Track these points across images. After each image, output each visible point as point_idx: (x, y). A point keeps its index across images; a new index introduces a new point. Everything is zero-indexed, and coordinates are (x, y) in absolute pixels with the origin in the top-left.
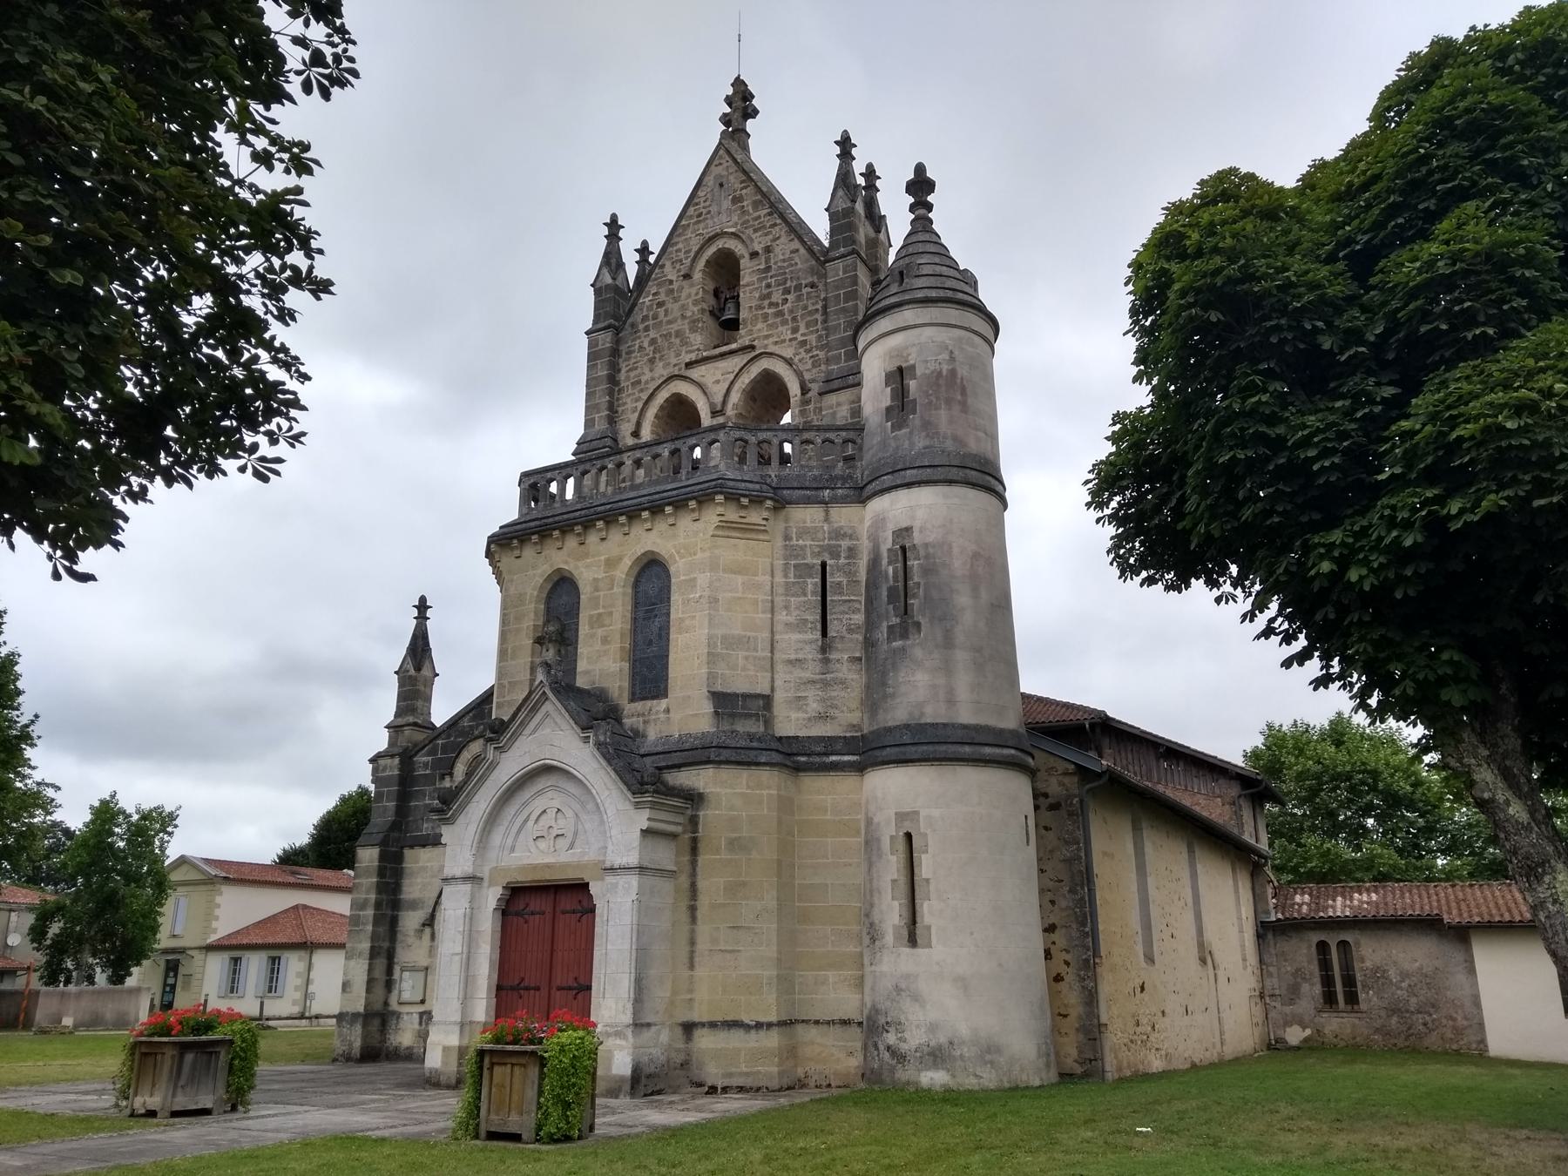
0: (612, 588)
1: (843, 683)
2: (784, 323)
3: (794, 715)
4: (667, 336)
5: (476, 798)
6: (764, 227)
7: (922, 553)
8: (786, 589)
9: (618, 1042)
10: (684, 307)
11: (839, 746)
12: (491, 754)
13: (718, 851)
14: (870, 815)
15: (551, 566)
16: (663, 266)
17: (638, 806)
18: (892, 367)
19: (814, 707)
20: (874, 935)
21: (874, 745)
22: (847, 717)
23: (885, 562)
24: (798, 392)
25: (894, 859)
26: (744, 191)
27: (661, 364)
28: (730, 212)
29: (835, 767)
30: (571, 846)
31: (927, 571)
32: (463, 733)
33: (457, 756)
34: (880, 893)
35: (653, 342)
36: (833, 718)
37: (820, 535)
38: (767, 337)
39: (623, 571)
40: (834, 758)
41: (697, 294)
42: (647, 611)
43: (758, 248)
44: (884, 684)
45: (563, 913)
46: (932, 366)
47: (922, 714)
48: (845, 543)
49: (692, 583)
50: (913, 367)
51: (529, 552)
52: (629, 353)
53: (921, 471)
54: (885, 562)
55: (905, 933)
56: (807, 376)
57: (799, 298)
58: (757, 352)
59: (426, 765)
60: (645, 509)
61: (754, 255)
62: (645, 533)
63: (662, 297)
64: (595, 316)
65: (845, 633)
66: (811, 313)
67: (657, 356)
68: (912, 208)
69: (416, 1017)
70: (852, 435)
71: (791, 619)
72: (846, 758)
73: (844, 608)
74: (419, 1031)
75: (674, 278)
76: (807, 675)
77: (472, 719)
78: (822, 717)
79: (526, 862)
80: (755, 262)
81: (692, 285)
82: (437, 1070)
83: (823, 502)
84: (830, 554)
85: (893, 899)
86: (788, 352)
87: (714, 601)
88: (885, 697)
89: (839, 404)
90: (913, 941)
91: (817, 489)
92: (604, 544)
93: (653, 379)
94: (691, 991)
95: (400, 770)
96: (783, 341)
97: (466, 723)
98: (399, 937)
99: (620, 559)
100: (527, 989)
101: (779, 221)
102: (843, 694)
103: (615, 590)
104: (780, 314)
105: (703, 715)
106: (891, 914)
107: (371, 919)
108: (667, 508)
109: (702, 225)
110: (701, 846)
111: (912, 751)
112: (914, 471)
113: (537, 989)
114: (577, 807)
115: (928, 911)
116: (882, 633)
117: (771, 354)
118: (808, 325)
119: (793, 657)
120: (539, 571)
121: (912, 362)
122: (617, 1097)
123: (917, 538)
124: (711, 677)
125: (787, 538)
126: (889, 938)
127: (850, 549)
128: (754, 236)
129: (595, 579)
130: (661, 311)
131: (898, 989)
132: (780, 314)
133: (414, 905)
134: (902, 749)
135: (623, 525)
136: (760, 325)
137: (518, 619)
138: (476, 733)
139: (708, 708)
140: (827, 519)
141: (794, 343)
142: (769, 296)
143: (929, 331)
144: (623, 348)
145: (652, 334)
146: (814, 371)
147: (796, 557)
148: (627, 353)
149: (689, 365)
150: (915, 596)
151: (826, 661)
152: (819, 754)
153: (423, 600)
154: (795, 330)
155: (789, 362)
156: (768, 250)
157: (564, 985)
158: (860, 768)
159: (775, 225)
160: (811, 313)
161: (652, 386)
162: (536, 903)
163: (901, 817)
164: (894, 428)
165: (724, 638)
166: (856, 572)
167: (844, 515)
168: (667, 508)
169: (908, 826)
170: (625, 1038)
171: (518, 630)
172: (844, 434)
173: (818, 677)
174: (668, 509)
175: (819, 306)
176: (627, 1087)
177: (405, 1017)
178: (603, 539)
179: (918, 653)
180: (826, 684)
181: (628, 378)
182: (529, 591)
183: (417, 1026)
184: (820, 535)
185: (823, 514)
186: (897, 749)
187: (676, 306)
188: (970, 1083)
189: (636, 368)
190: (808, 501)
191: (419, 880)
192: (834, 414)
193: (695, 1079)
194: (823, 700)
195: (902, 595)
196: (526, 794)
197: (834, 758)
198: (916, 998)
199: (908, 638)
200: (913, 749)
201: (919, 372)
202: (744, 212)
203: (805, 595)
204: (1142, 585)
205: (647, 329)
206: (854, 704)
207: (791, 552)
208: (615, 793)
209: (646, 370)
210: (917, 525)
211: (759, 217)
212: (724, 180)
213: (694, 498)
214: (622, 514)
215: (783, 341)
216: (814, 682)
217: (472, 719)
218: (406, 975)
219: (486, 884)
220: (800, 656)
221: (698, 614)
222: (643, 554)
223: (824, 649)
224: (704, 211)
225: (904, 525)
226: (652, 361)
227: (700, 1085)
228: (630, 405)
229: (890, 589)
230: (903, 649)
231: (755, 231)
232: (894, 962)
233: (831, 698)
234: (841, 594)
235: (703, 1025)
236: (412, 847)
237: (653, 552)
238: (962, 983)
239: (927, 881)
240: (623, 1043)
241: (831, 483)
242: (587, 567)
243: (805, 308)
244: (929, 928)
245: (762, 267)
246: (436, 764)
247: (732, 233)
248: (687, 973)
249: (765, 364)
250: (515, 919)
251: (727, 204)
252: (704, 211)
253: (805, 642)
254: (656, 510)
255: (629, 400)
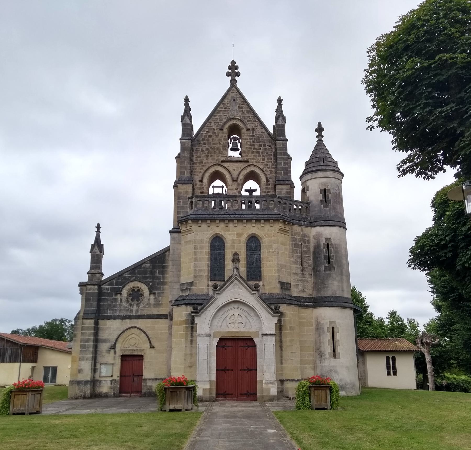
0: (240, 243)
1: (307, 281)
2: (260, 156)
3: (296, 290)
4: (213, 149)
5: (209, 309)
6: (251, 121)
7: (334, 246)
8: (293, 251)
9: (272, 385)
10: (219, 140)
11: (307, 300)
12: (216, 295)
13: (305, 332)
14: (319, 321)
15: (214, 232)
16: (210, 123)
17: (274, 316)
18: (323, 188)
19: (301, 288)
20: (321, 355)
21: (320, 301)
22: (309, 292)
23: (322, 247)
24: (265, 181)
25: (329, 334)
26: (243, 106)
27: (211, 158)
28: (238, 111)
29: (307, 306)
30: (245, 327)
31: (336, 252)
32: (125, 278)
33: (124, 287)
34: (324, 343)
35: (207, 149)
36: (305, 292)
37: (300, 235)
38: (253, 159)
39: (244, 238)
40: (306, 303)
41: (225, 137)
42: (251, 252)
43: (249, 127)
44: (323, 283)
45: (241, 347)
46: (335, 191)
47: (336, 293)
48: (307, 239)
49: (271, 246)
50: (329, 190)
51: (204, 226)
52: (197, 151)
53: (334, 222)
54: (322, 247)
55: (332, 354)
56: (268, 176)
57: (265, 149)
58: (250, 164)
59: (108, 289)
60: (254, 220)
61: (248, 130)
62: (252, 227)
63: (211, 134)
64: (182, 133)
65: (307, 266)
66: (269, 155)
67: (209, 155)
68: (317, 137)
69: (109, 382)
70: (307, 205)
71: (294, 260)
72: (310, 304)
73: (307, 258)
74: (111, 387)
75: (216, 128)
76: (298, 278)
77: (129, 274)
78: (303, 291)
79: (227, 330)
80: (248, 132)
81: (223, 133)
82: (201, 396)
83: (302, 225)
84: (303, 241)
85: (328, 345)
86: (262, 167)
87: (278, 253)
88: (324, 287)
89: (282, 189)
90: (335, 357)
91: (300, 221)
92: (236, 228)
93: (208, 163)
94: (282, 371)
95: (98, 290)
96: (260, 162)
97: (127, 275)
98: (98, 353)
99: (242, 234)
100: (228, 370)
101: (257, 120)
102: (307, 285)
103: (241, 244)
104: (258, 152)
105: (277, 288)
106: (328, 349)
107: (92, 346)
108: (262, 221)
109: (226, 112)
110: (283, 328)
111: (334, 304)
112: (332, 222)
113: (232, 370)
114: (246, 315)
115: (339, 349)
116: (322, 268)
117: (255, 166)
118: (268, 159)
119: (295, 272)
120: (209, 233)
121: (329, 188)
122: (273, 401)
123: (333, 242)
124: (279, 276)
125: (292, 235)
126: (327, 356)
127: (308, 241)
128: (248, 123)
129: (232, 239)
130: (210, 139)
131: (331, 370)
132: (258, 152)
133: (105, 341)
134: (331, 303)
135: (245, 223)
136: (250, 154)
137: (201, 248)
138: (132, 279)
139: (279, 286)
140: (302, 231)
141: (263, 164)
142: (254, 145)
143: (334, 180)
144: (195, 148)
145: (207, 146)
146: (271, 175)
147: (295, 241)
148: (196, 151)
149: (222, 161)
150: (333, 259)
151: (303, 274)
152: (303, 302)
153: (98, 225)
154: (264, 160)
155: (262, 170)
156: (253, 129)
157: (242, 369)
158: (313, 307)
159: (255, 121)
160: (269, 155)
161: (208, 166)
162: (229, 344)
163: (331, 322)
164: (324, 207)
165: (281, 265)
166: (310, 248)
167: (306, 230)
168: (262, 221)
169: (333, 325)
170: (274, 384)
171: (201, 252)
172: (305, 204)
173: (301, 279)
174: (263, 221)
175: (272, 154)
176: (276, 398)
177: (104, 382)
178: (235, 226)
179: (334, 276)
180: (303, 281)
181: (197, 160)
182: (205, 239)
183: (109, 385)
184: (300, 235)
185: (301, 229)
186: (330, 303)
187: (217, 139)
188: (350, 394)
189: (200, 157)
190: (298, 224)
191: (107, 332)
192: (281, 192)
193: (286, 396)
194: (303, 286)
195: (328, 258)
196: (226, 309)
197: (306, 303)
198: (336, 372)
199: (331, 271)
200: (335, 303)
201: (331, 192)
202: (243, 113)
203: (297, 253)
204: (412, 269)
205: (204, 144)
206: (310, 288)
207: (293, 240)
208: (265, 311)
209: (205, 159)
210: (332, 238)
211: (249, 117)
212: (235, 99)
213: (273, 220)
214: (245, 220)
215: (260, 162)
216: (300, 280)
217: (129, 274)
218: (103, 367)
219: (212, 337)
220: (297, 272)
221: (273, 256)
222: (251, 234)
223: (303, 270)
224: (227, 108)
225: (329, 237)
226: (207, 156)
227: (287, 397)
228: (198, 170)
229: (324, 256)
230: (330, 274)
231: (248, 121)
232: (329, 363)
233: (305, 286)
234: (306, 254)
235: (287, 380)
236: (103, 319)
237: (255, 234)
238: (347, 367)
239: (339, 340)
240: (274, 386)
241: (303, 219)
242: (229, 234)
243: (267, 153)
244: (339, 353)
245: (251, 134)
246: (113, 289)
247: (240, 120)
248: (280, 365)
249: (252, 168)
250: (221, 348)
251: (237, 108)
252: (227, 108)
253: (297, 268)
254: (258, 220)
255: (198, 168)
